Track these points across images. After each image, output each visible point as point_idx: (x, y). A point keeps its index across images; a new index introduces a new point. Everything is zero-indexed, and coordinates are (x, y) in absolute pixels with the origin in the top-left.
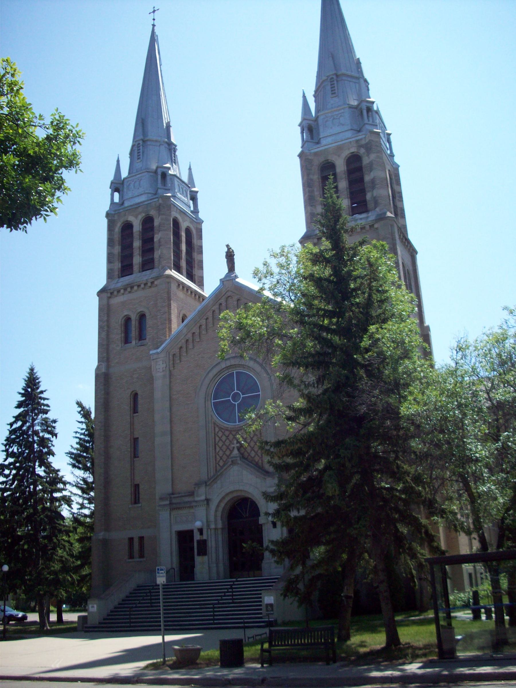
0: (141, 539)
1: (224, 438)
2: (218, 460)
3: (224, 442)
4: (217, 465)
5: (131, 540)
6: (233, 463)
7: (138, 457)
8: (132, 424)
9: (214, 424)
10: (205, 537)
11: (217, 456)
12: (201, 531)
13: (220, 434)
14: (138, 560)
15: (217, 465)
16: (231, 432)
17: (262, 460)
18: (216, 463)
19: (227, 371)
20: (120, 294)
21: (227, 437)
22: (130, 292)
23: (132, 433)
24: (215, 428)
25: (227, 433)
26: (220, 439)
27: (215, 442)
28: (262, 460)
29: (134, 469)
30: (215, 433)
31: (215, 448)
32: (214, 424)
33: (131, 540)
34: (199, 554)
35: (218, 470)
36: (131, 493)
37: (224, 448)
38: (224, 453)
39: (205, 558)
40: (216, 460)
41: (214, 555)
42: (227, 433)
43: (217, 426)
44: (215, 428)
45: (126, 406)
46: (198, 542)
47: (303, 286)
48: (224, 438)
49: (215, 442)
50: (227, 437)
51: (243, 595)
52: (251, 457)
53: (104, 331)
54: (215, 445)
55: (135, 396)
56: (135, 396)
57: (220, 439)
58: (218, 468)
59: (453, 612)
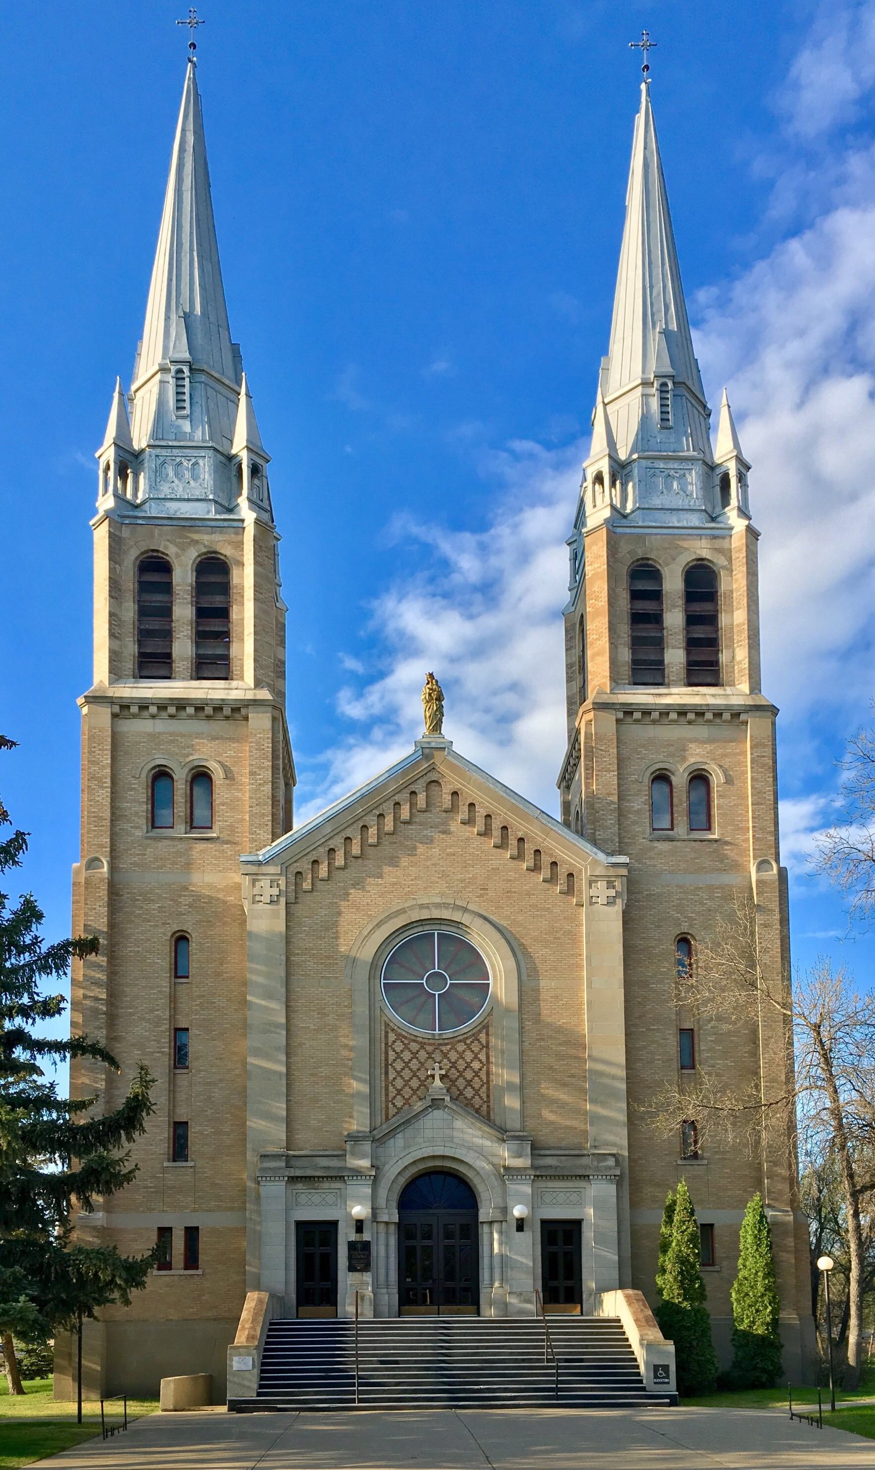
0: (192, 1233)
1: (407, 1056)
2: (391, 1095)
3: (407, 1064)
4: (390, 1105)
5: (165, 1232)
6: (436, 1104)
7: (187, 1068)
8: (173, 999)
9: (387, 1025)
10: (366, 1236)
11: (391, 1088)
12: (359, 1226)
13: (399, 1046)
14: (182, 1272)
15: (390, 1105)
16: (422, 1045)
17: (488, 1106)
18: (387, 1101)
19: (420, 929)
20: (145, 714)
21: (415, 1055)
22: (172, 716)
23: (173, 1018)
24: (387, 1033)
25: (414, 1046)
26: (398, 1056)
27: (387, 1059)
28: (488, 1106)
29: (174, 1092)
30: (386, 1044)
31: (387, 1073)
32: (387, 1025)
33: (165, 1232)
34: (352, 1268)
35: (390, 1116)
36: (169, 1138)
37: (407, 1074)
38: (407, 1083)
39: (367, 1277)
40: (387, 1095)
41: (382, 1272)
42: (414, 1046)
43: (393, 1030)
44: (387, 1033)
45: (162, 961)
46: (352, 1246)
47: (118, 854)
48: (407, 1056)
49: (387, 1059)
50: (415, 1055)
51: (587, 1347)
52: (466, 1098)
53: (103, 788)
54: (387, 1066)
55: (181, 939)
56: (181, 939)
57: (398, 1056)
58: (392, 1111)
59: (97, 1371)
